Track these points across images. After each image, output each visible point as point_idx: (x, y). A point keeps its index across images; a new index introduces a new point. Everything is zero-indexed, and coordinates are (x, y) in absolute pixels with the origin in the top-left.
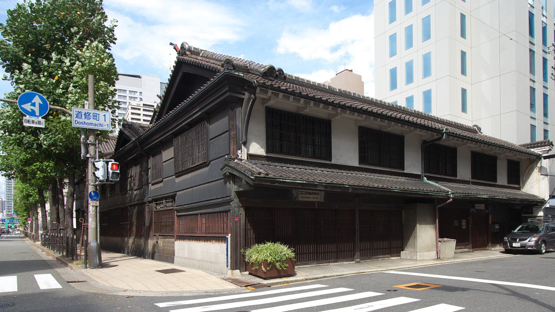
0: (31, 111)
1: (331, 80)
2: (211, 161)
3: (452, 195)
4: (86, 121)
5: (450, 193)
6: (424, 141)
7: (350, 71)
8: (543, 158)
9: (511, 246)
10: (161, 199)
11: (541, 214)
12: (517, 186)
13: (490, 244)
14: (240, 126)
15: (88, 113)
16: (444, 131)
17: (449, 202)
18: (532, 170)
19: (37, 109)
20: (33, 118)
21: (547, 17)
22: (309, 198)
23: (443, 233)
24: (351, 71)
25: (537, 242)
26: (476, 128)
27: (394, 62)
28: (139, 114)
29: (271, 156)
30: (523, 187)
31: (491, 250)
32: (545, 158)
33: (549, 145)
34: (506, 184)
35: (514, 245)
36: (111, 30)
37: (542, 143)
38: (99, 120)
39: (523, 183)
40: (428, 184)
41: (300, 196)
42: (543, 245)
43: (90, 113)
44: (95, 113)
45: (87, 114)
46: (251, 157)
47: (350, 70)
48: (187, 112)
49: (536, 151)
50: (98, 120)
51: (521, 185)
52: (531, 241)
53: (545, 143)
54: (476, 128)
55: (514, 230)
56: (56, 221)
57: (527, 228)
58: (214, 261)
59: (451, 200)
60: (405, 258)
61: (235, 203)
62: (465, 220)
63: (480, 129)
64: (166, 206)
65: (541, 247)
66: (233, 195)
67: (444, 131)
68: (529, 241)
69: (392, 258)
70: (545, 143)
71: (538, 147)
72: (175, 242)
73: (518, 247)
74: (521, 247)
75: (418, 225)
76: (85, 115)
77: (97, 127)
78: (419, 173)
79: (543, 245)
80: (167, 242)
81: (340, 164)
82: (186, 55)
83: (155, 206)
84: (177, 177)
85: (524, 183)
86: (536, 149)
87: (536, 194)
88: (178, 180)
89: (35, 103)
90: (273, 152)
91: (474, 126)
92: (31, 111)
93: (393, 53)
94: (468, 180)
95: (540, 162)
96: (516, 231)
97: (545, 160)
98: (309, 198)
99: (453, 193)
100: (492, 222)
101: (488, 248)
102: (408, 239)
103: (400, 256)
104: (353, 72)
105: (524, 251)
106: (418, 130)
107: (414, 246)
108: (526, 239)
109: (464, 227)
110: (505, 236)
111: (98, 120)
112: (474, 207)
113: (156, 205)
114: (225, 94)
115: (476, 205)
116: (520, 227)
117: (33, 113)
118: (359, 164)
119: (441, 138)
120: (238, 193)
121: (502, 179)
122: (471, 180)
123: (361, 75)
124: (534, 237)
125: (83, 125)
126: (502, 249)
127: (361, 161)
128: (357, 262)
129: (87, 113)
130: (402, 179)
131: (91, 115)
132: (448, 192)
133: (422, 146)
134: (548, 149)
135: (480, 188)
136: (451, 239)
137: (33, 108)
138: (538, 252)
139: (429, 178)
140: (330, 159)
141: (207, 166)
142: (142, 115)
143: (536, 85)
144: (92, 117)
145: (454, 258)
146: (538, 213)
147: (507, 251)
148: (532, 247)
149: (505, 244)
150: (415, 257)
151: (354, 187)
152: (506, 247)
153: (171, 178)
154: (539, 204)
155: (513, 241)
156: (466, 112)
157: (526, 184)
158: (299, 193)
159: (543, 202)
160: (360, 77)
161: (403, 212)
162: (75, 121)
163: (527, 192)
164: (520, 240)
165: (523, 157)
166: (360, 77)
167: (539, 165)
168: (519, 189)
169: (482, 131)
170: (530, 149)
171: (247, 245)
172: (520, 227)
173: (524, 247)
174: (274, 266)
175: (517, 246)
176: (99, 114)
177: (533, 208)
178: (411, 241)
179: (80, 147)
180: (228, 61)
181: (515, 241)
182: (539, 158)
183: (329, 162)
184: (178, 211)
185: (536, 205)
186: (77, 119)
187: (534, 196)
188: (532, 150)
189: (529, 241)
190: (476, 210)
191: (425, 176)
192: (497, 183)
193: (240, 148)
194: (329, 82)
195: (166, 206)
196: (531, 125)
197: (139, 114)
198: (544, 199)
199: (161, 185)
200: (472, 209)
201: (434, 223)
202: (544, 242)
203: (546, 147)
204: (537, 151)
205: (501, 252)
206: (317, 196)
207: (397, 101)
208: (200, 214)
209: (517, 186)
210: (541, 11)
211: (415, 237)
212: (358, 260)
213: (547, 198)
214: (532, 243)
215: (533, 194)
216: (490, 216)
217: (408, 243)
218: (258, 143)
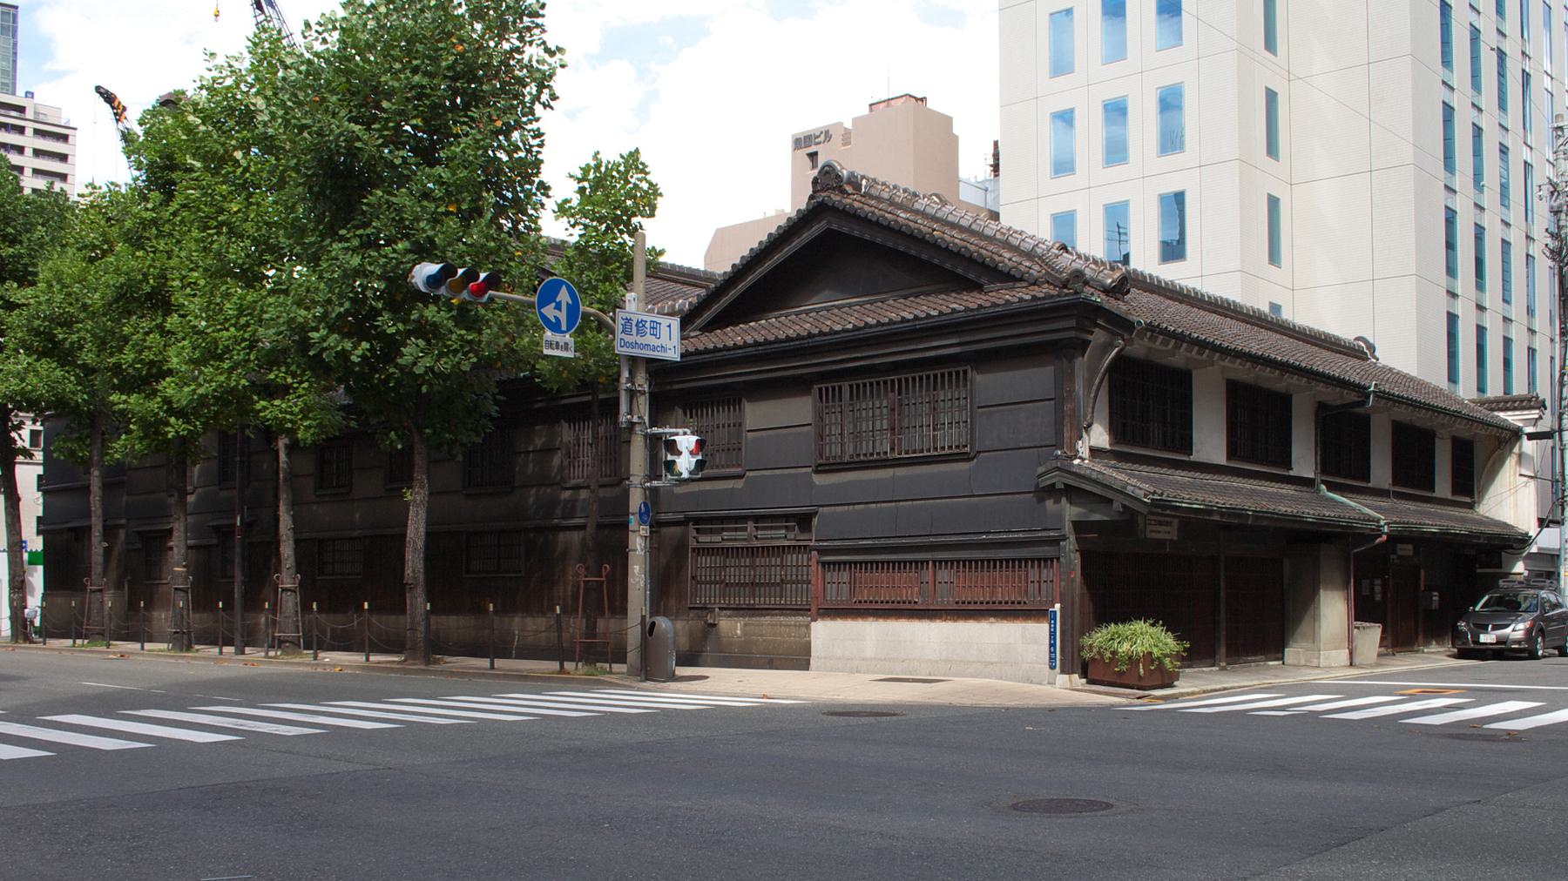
0: (554, 321)
1: (855, 121)
2: (979, 452)
3: (1386, 527)
4: (640, 340)
5: (1382, 523)
6: (1320, 403)
7: (917, 99)
8: (1525, 437)
9: (1477, 642)
10: (745, 519)
11: (1519, 567)
12: (1468, 500)
13: (1421, 638)
14: (1081, 392)
16: (1372, 389)
18: (1500, 462)
19: (563, 316)
20: (558, 338)
21: (1531, 56)
22: (1159, 532)
23: (1363, 611)
24: (923, 100)
25: (1528, 632)
26: (1363, 345)
27: (1063, 93)
28: (38, 153)
29: (1174, 457)
30: (1479, 503)
31: (1423, 652)
32: (1531, 437)
33: (1539, 408)
34: (1450, 496)
35: (1483, 638)
37: (1522, 401)
39: (1479, 493)
40: (1332, 500)
41: (1150, 528)
42: (1540, 640)
46: (1095, 452)
47: (919, 96)
48: (903, 340)
49: (1509, 419)
51: (1476, 499)
52: (1516, 630)
53: (1530, 401)
54: (1363, 345)
55: (1475, 605)
56: (184, 567)
57: (1500, 601)
58: (996, 660)
59: (1385, 537)
60: (1295, 662)
61: (1070, 544)
63: (1372, 348)
64: (756, 538)
65: (1537, 642)
66: (1068, 528)
67: (1372, 389)
68: (1514, 630)
69: (1271, 663)
70: (1530, 401)
71: (1515, 409)
72: (813, 623)
73: (1491, 644)
74: (1498, 643)
75: (1321, 591)
77: (656, 353)
78: (1312, 476)
79: (1540, 640)
80: (795, 626)
81: (1201, 460)
82: (843, 192)
83: (695, 534)
84: (817, 472)
85: (1483, 490)
86: (1510, 413)
87: (1509, 522)
88: (818, 480)
89: (560, 302)
91: (1357, 339)
92: (554, 321)
93: (1061, 66)
94: (1387, 487)
95: (1517, 446)
96: (1478, 608)
97: (1531, 442)
98: (1159, 532)
99: (1388, 524)
100: (1425, 586)
101: (1416, 648)
102: (1298, 620)
103: (1282, 659)
105: (1502, 652)
106: (1322, 384)
107: (1314, 637)
108: (1506, 626)
109: (1378, 598)
110: (1460, 618)
112: (1394, 552)
113: (698, 533)
114: (1061, 329)
115: (1399, 546)
116: (1486, 598)
117: (555, 327)
118: (1229, 458)
119: (1363, 403)
120: (1079, 526)
122: (1392, 489)
123: (950, 115)
124: (1523, 621)
125: (634, 350)
126: (1448, 648)
127: (1231, 454)
128: (1223, 669)
130: (1288, 490)
131: (647, 325)
132: (1378, 520)
133: (1317, 415)
134: (1537, 416)
135: (1413, 508)
136: (1372, 624)
137: (557, 313)
138: (1532, 655)
139: (1332, 487)
141: (970, 459)
142: (29, 152)
143: (1458, 201)
145: (1378, 665)
146: (1513, 567)
147: (1463, 654)
148: (1519, 642)
149: (1457, 636)
150: (1316, 661)
151: (1258, 515)
152: (1463, 643)
153: (804, 470)
155: (1480, 631)
156: (1279, 262)
157: (1487, 497)
158: (1148, 522)
159: (1525, 540)
161: (1286, 562)
163: (1487, 515)
164: (1495, 628)
165: (1480, 431)
167: (1516, 450)
168: (1471, 506)
169: (1377, 354)
170: (1496, 413)
171: (1087, 629)
172: (1486, 598)
173: (1504, 643)
174: (1161, 664)
175: (1489, 641)
178: (1305, 626)
179: (618, 399)
181: (1484, 629)
182: (1516, 434)
183: (1429, 494)
184: (822, 551)
185: (1511, 547)
186: (623, 336)
187: (1505, 525)
188: (1502, 415)
189: (1514, 630)
190: (1400, 557)
191: (1323, 482)
192: (1434, 495)
193: (1080, 437)
194: (848, 125)
195: (756, 538)
197: (38, 153)
198: (1527, 534)
199: (739, 484)
200: (1392, 556)
201: (1346, 587)
202: (1542, 632)
203: (1533, 412)
204: (1512, 418)
205: (1449, 656)
206: (1168, 529)
207: (1075, 211)
208: (934, 562)
209: (1468, 500)
210: (1520, 43)
211: (1316, 618)
212: (1223, 664)
213: (1531, 528)
214: (1519, 635)
215: (1502, 519)
216: (1422, 572)
217: (1299, 631)
218: (1101, 424)
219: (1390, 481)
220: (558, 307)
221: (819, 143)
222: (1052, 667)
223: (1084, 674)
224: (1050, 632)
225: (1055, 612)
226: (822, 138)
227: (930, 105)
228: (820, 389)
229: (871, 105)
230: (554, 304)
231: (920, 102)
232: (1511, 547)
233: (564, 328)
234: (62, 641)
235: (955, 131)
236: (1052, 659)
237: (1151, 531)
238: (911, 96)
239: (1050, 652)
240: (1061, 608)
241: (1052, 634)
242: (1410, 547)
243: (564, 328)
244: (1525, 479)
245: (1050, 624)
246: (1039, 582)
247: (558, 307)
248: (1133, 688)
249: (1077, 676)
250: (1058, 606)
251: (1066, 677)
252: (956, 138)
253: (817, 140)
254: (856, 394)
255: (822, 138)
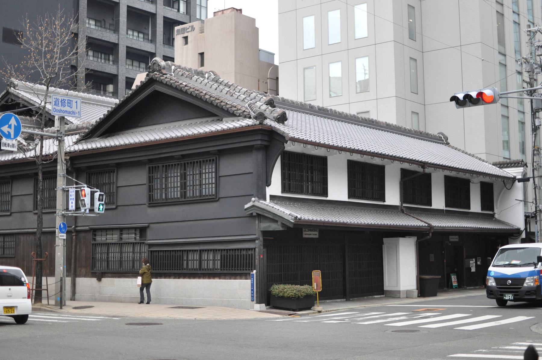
0: (7, 133)
4: (63, 109)
7: (237, 10)
8: (517, 181)
15: (64, 99)
17: (528, 316)
22: (311, 234)
24: (241, 10)
36: (464, 288)
38: (72, 108)
43: (65, 100)
44: (69, 100)
45: (63, 101)
47: (238, 8)
50: (71, 107)
62: (319, 272)
76: (61, 102)
90: (289, 191)
92: (7, 133)
94: (442, 208)
98: (311, 234)
104: (243, 13)
111: (71, 107)
115: (450, 237)
117: (8, 136)
118: (349, 198)
121: (476, 206)
122: (445, 208)
127: (351, 195)
129: (63, 99)
137: (9, 130)
140: (325, 194)
144: (67, 104)
150: (398, 295)
154: (514, 235)
160: (253, 20)
162: (54, 108)
166: (253, 20)
176: (72, 101)
177: (509, 239)
180: (261, 114)
190: (451, 242)
196: (408, 5)
200: (446, 242)
219: (444, 205)
220: (10, 127)
221: (189, 32)
222: (253, 301)
223: (268, 304)
224: (251, 284)
225: (253, 274)
226: (190, 30)
227: (244, 13)
228: (149, 168)
229: (214, 13)
230: (7, 126)
231: (239, 11)
232: (513, 236)
233: (12, 136)
234: (188, 318)
235: (257, 26)
236: (252, 297)
237: (306, 234)
238: (234, 8)
239: (252, 293)
240: (256, 273)
241: (252, 285)
242: (457, 237)
243: (12, 136)
244: (519, 201)
245: (251, 280)
246: (214, 260)
247: (10, 127)
248: (290, 310)
249: (264, 305)
250: (255, 271)
251: (43, 301)
252: (257, 29)
253: (188, 30)
254: (167, 168)
255: (190, 30)
